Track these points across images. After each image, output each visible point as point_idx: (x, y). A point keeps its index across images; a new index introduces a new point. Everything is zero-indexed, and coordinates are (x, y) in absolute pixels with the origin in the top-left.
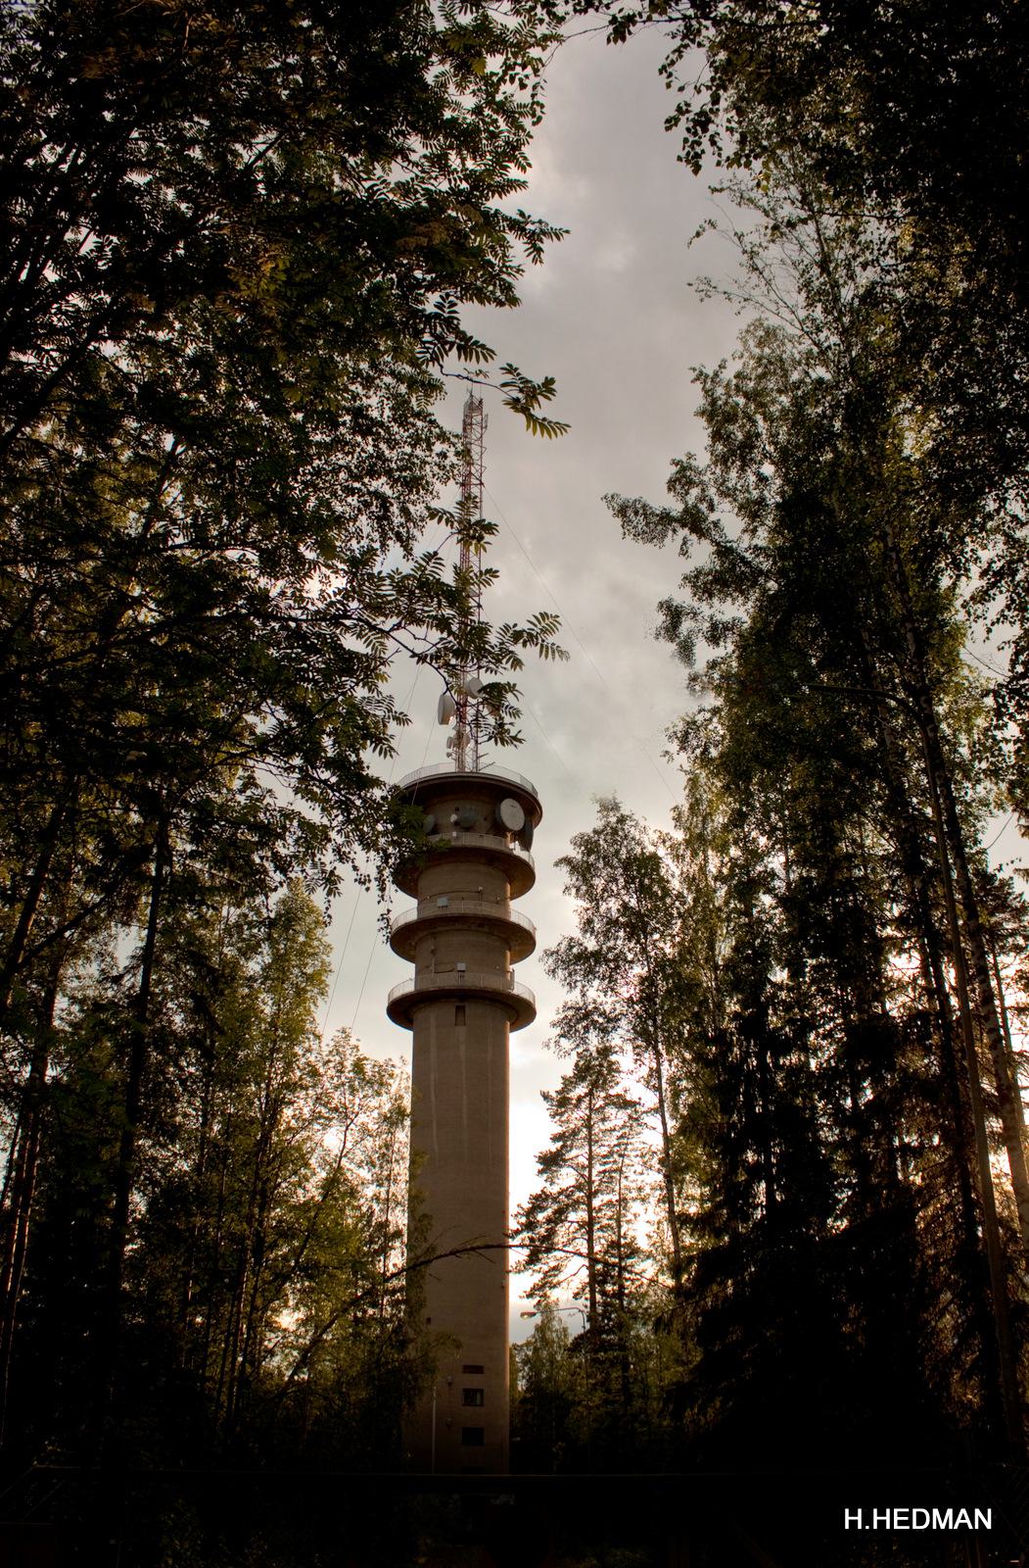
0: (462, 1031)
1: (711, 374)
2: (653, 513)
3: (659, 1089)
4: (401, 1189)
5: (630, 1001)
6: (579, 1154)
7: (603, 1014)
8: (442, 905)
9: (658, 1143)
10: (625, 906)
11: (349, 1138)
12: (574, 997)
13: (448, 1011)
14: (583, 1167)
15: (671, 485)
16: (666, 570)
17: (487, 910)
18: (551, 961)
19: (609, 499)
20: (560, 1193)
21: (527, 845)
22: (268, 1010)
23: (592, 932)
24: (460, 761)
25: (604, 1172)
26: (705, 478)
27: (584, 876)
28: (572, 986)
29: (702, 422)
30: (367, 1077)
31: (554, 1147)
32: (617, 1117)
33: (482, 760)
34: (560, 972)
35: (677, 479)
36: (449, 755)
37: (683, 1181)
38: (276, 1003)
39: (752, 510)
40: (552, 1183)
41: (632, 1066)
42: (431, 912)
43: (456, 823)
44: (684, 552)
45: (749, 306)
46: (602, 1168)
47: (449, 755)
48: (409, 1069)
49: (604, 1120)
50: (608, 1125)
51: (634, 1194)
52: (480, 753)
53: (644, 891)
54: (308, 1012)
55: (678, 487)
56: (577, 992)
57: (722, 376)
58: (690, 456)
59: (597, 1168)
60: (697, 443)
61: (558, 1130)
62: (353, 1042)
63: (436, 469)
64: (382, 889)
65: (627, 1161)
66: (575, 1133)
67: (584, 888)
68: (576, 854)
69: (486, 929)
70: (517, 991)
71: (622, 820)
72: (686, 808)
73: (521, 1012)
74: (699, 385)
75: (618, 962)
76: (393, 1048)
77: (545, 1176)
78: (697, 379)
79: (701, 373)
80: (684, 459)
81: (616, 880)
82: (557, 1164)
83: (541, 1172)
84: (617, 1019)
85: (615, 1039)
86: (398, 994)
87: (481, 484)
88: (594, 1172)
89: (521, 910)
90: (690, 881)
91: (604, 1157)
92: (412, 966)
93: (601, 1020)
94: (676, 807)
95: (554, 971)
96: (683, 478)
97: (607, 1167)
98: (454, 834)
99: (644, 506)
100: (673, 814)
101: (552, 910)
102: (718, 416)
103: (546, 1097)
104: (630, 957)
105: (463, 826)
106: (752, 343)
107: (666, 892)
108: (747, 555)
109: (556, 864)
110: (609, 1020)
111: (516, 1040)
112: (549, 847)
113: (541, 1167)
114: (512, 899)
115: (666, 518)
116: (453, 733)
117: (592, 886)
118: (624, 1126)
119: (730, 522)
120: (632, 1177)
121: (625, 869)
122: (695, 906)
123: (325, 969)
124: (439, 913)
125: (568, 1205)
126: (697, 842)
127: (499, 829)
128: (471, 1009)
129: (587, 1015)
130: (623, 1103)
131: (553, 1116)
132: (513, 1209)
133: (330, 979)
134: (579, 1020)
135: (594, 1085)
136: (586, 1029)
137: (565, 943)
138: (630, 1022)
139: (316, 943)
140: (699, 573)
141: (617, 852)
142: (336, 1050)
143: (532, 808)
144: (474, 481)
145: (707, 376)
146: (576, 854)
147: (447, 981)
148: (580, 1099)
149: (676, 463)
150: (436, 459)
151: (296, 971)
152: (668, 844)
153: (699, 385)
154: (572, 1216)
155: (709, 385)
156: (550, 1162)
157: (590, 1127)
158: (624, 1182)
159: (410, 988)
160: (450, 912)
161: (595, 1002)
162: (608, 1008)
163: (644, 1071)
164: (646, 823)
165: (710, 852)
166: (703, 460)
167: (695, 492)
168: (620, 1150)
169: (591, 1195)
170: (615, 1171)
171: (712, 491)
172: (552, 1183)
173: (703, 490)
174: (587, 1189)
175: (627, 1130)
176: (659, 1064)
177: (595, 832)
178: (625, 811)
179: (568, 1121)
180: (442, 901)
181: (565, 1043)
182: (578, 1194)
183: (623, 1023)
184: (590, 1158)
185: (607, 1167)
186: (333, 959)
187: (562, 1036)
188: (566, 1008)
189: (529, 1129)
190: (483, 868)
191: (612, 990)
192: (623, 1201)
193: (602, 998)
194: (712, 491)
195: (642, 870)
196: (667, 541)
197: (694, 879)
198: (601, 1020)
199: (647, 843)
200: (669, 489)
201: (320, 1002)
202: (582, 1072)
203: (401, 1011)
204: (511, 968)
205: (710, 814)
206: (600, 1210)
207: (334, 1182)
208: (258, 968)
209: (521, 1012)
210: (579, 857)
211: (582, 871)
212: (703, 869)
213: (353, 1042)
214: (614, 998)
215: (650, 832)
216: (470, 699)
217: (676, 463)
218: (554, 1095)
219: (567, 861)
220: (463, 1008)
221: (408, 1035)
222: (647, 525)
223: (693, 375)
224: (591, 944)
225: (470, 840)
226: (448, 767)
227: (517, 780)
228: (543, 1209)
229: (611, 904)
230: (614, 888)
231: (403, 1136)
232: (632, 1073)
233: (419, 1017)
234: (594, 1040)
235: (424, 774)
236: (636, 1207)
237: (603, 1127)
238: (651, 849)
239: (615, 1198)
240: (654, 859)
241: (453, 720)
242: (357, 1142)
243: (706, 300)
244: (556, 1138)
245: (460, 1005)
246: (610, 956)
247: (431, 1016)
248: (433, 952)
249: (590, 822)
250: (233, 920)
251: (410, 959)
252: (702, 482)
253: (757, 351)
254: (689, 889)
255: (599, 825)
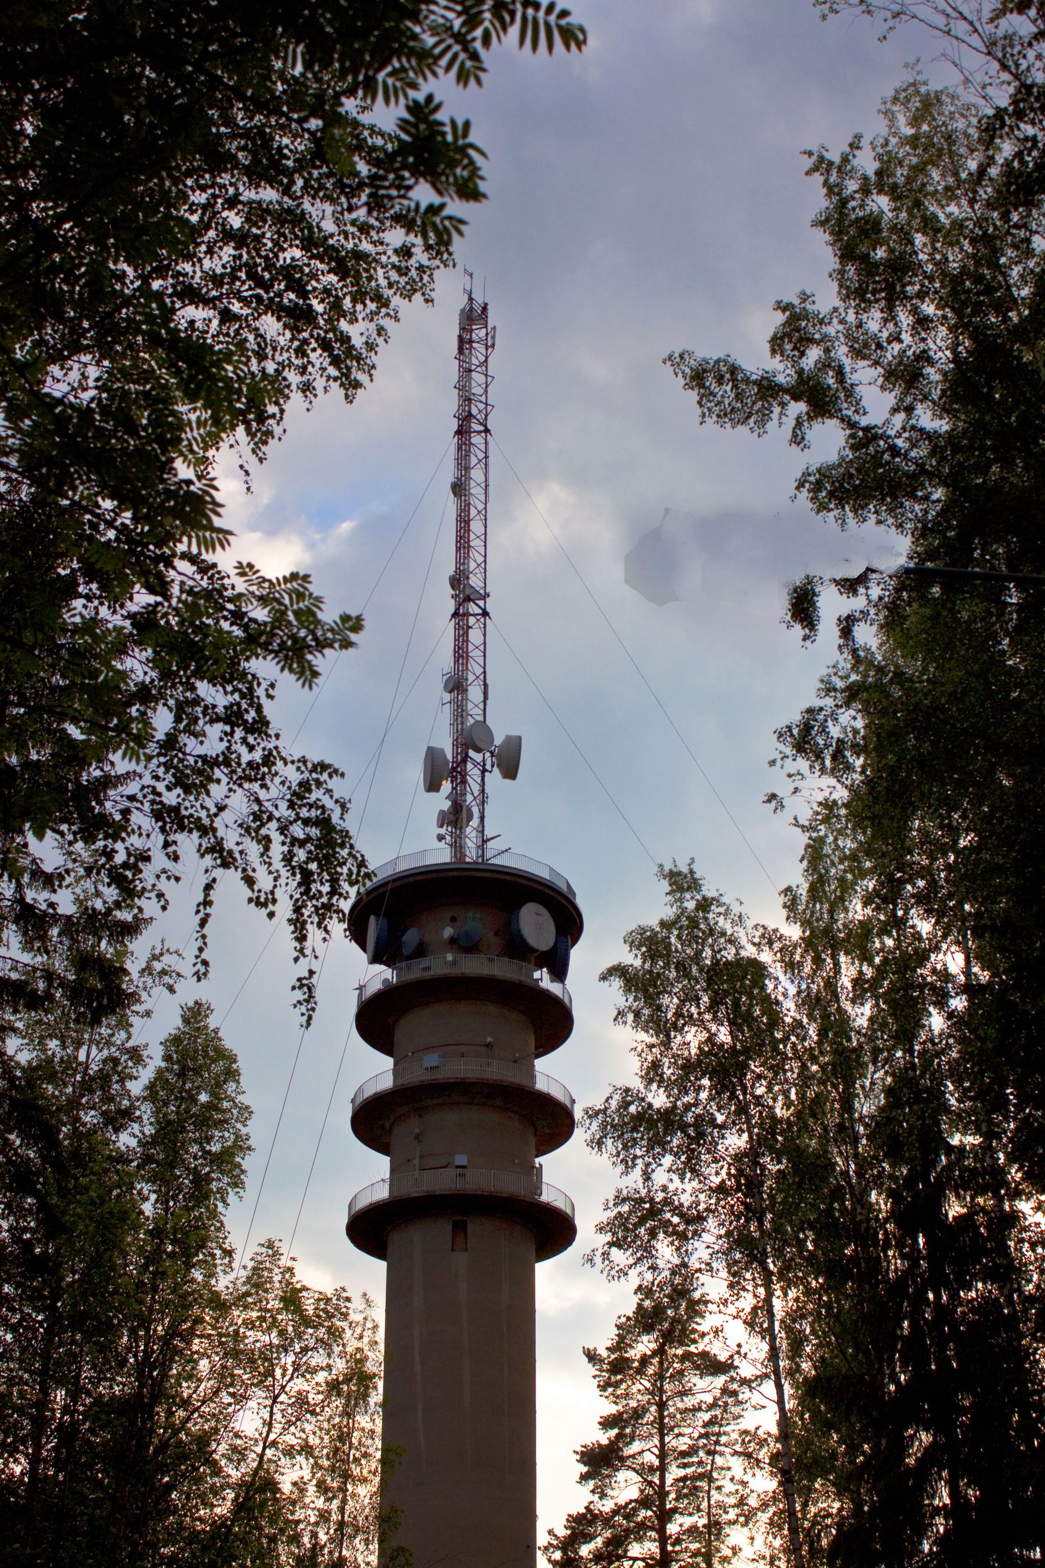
0: (462, 1259)
1: (837, 160)
2: (747, 381)
3: (768, 1333)
4: (364, 1494)
5: (721, 1189)
6: (644, 1449)
7: (678, 1210)
8: (434, 1066)
9: (768, 1421)
10: (711, 1039)
11: (278, 1416)
12: (634, 1180)
13: (440, 1230)
14: (652, 1469)
15: (776, 344)
16: (778, 458)
17: (496, 1071)
18: (595, 1126)
19: (676, 360)
20: (615, 1512)
21: (559, 973)
22: (148, 1208)
23: (661, 1082)
24: (458, 847)
25: (684, 1479)
26: (831, 330)
27: (645, 991)
28: (628, 1166)
29: (822, 237)
30: (312, 1319)
31: (604, 1438)
32: (706, 1388)
33: (490, 844)
34: (609, 1142)
35: (785, 335)
36: (441, 838)
37: (810, 1489)
38: (163, 1200)
39: (906, 375)
40: (603, 1496)
41: (725, 1293)
42: (415, 1076)
43: (453, 941)
44: (798, 439)
45: (905, 26)
46: (682, 1473)
47: (441, 838)
48: (379, 1314)
49: (683, 1393)
50: (689, 1402)
51: (732, 1515)
52: (488, 833)
53: (738, 1021)
54: (214, 1214)
55: (788, 347)
56: (637, 1173)
57: (855, 162)
58: (805, 297)
59: (674, 1472)
60: (813, 270)
61: (611, 1409)
62: (284, 1261)
63: (394, 276)
64: (302, 938)
65: (719, 1461)
66: (637, 1414)
67: (646, 1011)
68: (633, 960)
69: (498, 1102)
70: (547, 1196)
71: (704, 905)
72: (803, 891)
73: (553, 1231)
74: (818, 178)
75: (699, 1135)
76: (363, 1284)
77: (591, 1484)
78: (815, 169)
79: (821, 159)
80: (796, 301)
81: (697, 999)
82: (609, 1464)
83: (584, 1478)
84: (700, 1219)
85: (700, 1250)
86: (362, 1203)
87: (487, 431)
88: (669, 1480)
89: (553, 1072)
90: (811, 1002)
91: (683, 1454)
92: (386, 1160)
93: (676, 1220)
94: (789, 889)
95: (600, 1143)
96: (795, 331)
97: (689, 1471)
98: (450, 957)
99: (734, 370)
100: (782, 899)
101: (600, 1057)
102: (851, 235)
103: (592, 1357)
104: (720, 1118)
105: (464, 945)
106: (902, 120)
107: (775, 1020)
108: (900, 442)
109: (604, 978)
110: (688, 1222)
111: (545, 1271)
112: (589, 984)
113: (584, 1469)
114: (538, 1056)
115: (769, 389)
116: (446, 805)
117: (659, 1008)
118: (711, 1407)
119: (876, 403)
120: (729, 1487)
121: (710, 981)
122: (819, 1043)
123: (241, 1145)
124: (427, 1077)
125: (627, 1531)
126: (822, 940)
127: (517, 948)
128: (477, 1228)
129: (654, 1212)
130: (712, 1366)
131: (603, 1388)
132: (542, 1539)
133: (247, 1162)
134: (640, 1221)
135: (668, 1338)
136: (653, 1234)
137: (617, 1097)
138: (722, 1224)
139: (226, 1104)
140: (824, 473)
141: (698, 956)
142: (257, 1280)
143: (569, 923)
144: (476, 427)
145: (831, 163)
146: (633, 960)
147: (440, 1182)
148: (644, 1360)
149: (783, 307)
150: (395, 259)
151: (195, 1149)
152: (777, 946)
153: (818, 178)
154: (635, 1550)
155: (833, 178)
156: (599, 1462)
157: (662, 1406)
158: (716, 1496)
159: (383, 1193)
160: (441, 1076)
161: (664, 1189)
162: (686, 1199)
163: (747, 1302)
164: (743, 910)
165: (842, 958)
166: (827, 298)
167: (813, 355)
168: (711, 1439)
169: (665, 1516)
170: (701, 1477)
171: (841, 352)
172: (603, 1496)
173: (827, 351)
174: (656, 1501)
175: (718, 1412)
176: (770, 1294)
177: (663, 924)
178: (709, 890)
179: (627, 1395)
180: (431, 1060)
181: (619, 1256)
182: (643, 1514)
183: (711, 1223)
184: (662, 1456)
185: (689, 1471)
186: (255, 1130)
187: (611, 1244)
188: (620, 1200)
189: (568, 1408)
190: (492, 1009)
191: (693, 1171)
192: (715, 1528)
193: (676, 1184)
194: (841, 352)
195: (735, 985)
196: (771, 426)
197: (818, 999)
198: (676, 1220)
199: (744, 941)
200: (773, 351)
201: (231, 1198)
202: (645, 1319)
203: (369, 1229)
204: (538, 1160)
205: (842, 899)
206: (678, 1541)
207: (259, 1489)
208: (133, 1143)
209: (553, 1231)
210: (638, 963)
211: (642, 986)
212: (831, 985)
213: (284, 1261)
214: (695, 1184)
215: (750, 924)
216: (472, 753)
217: (783, 307)
218: (604, 1353)
219: (619, 971)
220: (465, 1223)
221: (380, 1267)
222: (739, 397)
223: (809, 163)
224: (659, 1099)
225: (474, 966)
226: (441, 855)
227: (544, 874)
228: (589, 1538)
229: (689, 1037)
230: (694, 1010)
231: (370, 1422)
232: (727, 1326)
233: (396, 1240)
234: (665, 1251)
235: (402, 867)
236: (736, 1536)
237: (680, 1405)
238: (749, 952)
239: (702, 1522)
240: (758, 970)
241: (446, 786)
242: (290, 1423)
243: (831, 16)
244: (607, 1423)
245: (461, 1218)
246: (689, 1118)
247: (421, 1238)
248: (418, 1138)
249: (655, 908)
250: (94, 1068)
251: (387, 1154)
252: (825, 338)
253: (910, 131)
254: (811, 1017)
255: (669, 913)
